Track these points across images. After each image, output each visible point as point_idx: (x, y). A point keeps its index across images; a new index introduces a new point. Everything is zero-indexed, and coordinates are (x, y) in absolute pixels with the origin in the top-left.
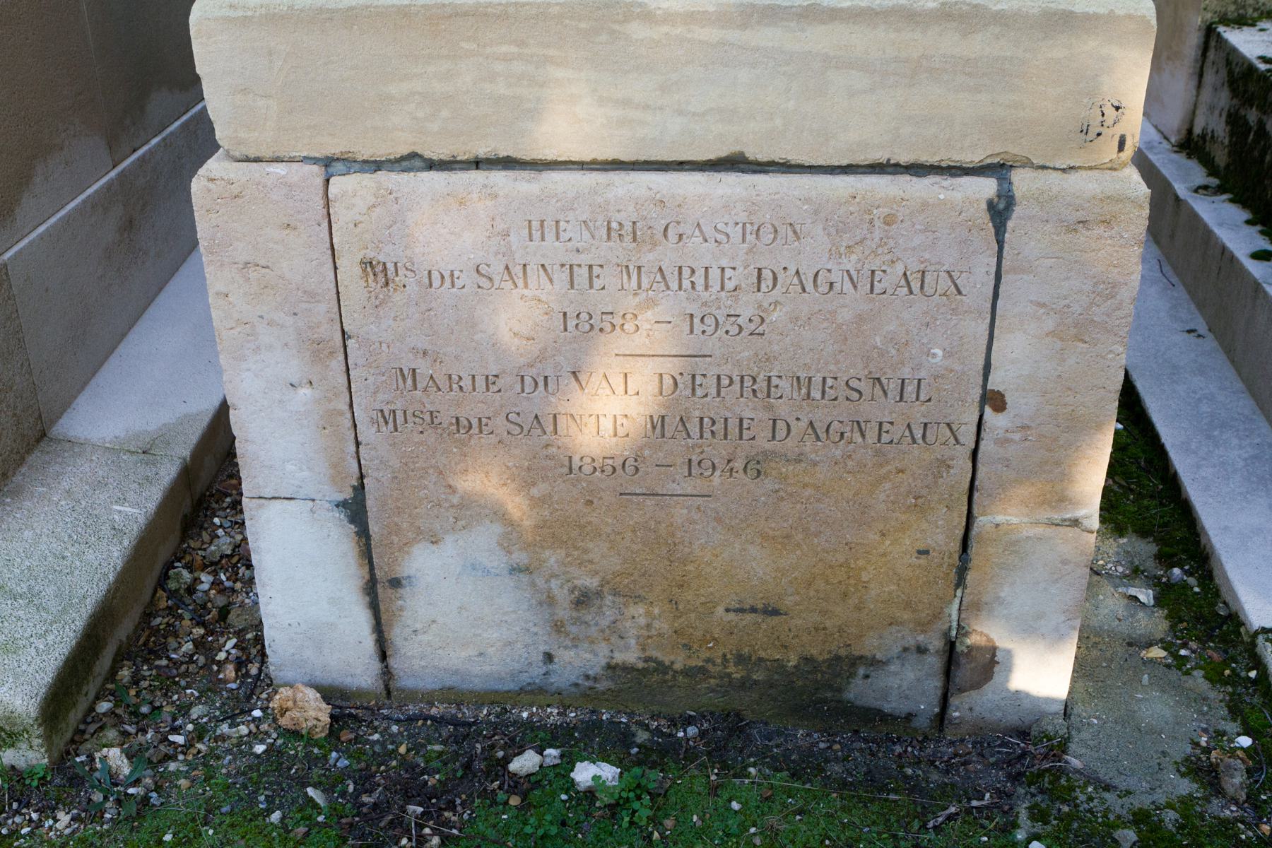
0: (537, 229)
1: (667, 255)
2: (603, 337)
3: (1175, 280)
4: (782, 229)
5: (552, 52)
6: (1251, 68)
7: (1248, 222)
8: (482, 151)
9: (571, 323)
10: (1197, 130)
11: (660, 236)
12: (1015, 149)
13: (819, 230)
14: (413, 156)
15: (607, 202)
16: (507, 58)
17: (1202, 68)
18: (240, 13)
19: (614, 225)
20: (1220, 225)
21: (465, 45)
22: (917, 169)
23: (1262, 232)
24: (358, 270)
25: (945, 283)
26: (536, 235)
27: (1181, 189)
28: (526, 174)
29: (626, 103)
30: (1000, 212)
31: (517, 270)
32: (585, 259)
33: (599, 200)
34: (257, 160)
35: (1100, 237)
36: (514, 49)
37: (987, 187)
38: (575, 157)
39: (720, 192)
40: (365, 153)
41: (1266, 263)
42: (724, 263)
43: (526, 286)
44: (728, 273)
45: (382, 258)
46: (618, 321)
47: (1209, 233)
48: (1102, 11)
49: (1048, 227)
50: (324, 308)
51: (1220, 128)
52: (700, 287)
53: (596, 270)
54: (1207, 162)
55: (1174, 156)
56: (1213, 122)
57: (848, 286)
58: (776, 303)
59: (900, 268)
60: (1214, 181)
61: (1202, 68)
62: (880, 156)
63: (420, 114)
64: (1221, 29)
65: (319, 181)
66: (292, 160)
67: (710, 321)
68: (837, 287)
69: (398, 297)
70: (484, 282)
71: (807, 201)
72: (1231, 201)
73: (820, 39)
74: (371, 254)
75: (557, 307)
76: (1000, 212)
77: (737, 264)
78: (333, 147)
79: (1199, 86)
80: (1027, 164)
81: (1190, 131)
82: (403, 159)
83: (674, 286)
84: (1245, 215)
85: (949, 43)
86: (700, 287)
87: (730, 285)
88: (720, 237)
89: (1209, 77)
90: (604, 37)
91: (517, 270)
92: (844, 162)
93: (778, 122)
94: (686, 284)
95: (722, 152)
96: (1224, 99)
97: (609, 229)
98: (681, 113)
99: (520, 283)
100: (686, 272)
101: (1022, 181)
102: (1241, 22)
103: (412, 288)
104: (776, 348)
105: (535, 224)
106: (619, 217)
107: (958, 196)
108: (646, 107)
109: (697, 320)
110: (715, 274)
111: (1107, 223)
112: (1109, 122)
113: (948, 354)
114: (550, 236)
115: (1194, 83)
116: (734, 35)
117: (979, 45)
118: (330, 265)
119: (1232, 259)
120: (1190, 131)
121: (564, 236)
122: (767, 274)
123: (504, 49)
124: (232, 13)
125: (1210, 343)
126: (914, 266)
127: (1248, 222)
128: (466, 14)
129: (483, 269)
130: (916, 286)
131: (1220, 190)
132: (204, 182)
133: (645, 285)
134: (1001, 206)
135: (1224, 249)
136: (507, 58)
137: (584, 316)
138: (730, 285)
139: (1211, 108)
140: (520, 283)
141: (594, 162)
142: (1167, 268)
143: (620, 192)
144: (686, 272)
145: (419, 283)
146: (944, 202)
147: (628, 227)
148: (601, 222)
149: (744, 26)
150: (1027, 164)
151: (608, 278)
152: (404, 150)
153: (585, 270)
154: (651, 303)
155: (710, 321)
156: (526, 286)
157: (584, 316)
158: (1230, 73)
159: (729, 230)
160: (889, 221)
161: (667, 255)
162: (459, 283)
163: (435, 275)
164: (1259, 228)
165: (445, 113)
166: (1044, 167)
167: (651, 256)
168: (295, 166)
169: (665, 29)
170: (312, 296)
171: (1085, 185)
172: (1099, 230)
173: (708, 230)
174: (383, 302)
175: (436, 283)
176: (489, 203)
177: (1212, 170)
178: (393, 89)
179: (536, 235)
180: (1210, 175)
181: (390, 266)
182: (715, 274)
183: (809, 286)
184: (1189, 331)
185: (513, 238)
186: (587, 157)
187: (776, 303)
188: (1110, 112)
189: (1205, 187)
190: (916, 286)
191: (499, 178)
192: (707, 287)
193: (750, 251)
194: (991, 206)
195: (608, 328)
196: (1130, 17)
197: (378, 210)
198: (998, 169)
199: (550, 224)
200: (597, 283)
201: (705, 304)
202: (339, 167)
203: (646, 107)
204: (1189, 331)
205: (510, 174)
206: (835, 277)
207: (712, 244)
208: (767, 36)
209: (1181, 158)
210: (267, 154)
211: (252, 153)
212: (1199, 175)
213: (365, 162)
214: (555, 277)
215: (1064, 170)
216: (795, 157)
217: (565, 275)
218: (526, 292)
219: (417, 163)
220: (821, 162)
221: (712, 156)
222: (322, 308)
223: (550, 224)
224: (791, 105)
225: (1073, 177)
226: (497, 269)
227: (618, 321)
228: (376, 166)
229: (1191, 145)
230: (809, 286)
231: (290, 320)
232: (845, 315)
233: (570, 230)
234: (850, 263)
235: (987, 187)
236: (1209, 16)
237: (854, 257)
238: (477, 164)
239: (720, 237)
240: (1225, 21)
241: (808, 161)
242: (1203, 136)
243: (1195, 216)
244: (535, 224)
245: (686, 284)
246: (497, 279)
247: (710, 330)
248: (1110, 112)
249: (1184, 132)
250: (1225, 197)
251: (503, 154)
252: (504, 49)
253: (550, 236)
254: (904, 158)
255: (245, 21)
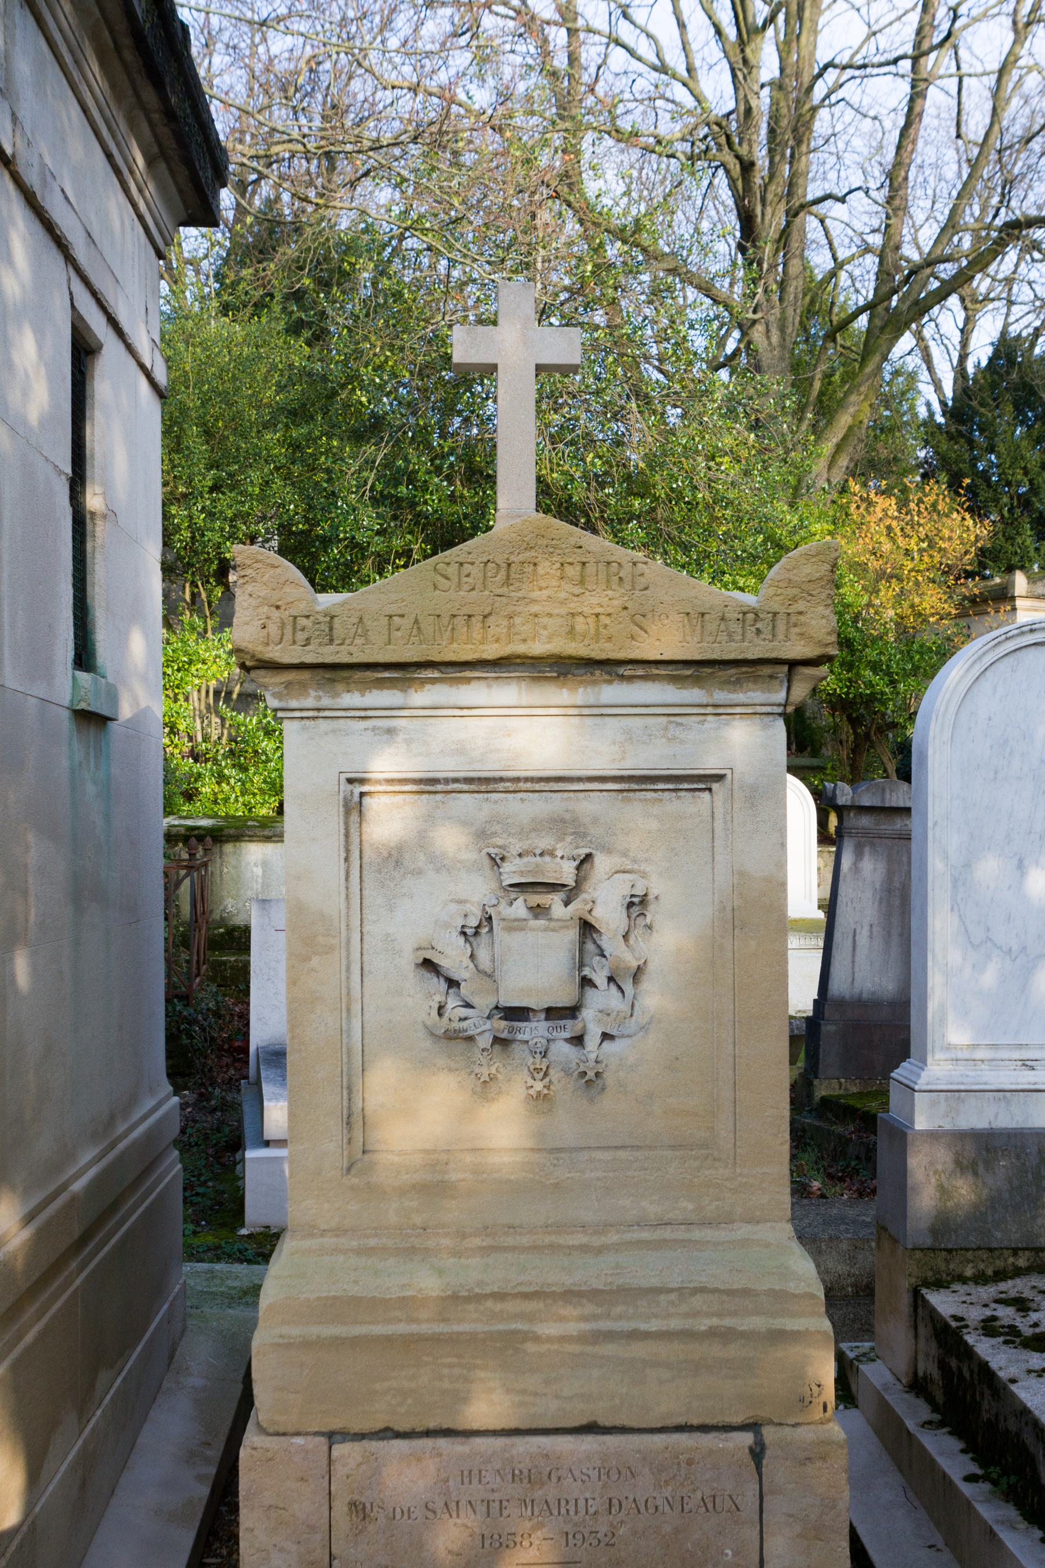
0: (467, 1476)
1: (550, 1492)
2: (508, 1551)
3: (916, 1503)
4: (623, 1471)
5: (479, 1362)
6: (947, 1325)
7: (963, 1451)
8: (432, 1424)
9: (487, 1542)
10: (921, 1374)
11: (545, 1478)
12: (763, 1413)
13: (647, 1470)
14: (387, 1429)
15: (512, 1457)
16: (451, 1366)
17: (915, 1321)
18: (286, 1341)
19: (517, 1472)
20: (941, 1454)
21: (425, 1358)
22: (704, 1428)
23: (973, 1459)
24: (346, 1509)
25: (728, 1503)
26: (466, 1480)
27: (910, 1424)
28: (459, 1440)
29: (524, 1392)
30: (757, 1453)
31: (453, 1506)
32: (497, 1496)
33: (507, 1455)
34: (284, 1434)
35: (820, 1469)
36: (455, 1360)
37: (747, 1439)
38: (491, 1427)
39: (583, 1448)
40: (356, 1427)
41: (975, 1484)
42: (588, 1495)
43: (458, 1516)
44: (590, 1502)
45: (363, 1500)
46: (518, 1539)
47: (933, 1461)
48: (802, 1329)
49: (788, 1463)
50: (318, 1539)
51: (935, 1373)
52: (572, 1513)
53: (505, 1503)
54: (930, 1400)
55: (906, 1396)
56: (928, 1367)
57: (667, 1508)
58: (622, 1522)
59: (699, 1495)
60: (937, 1417)
61: (915, 1321)
62: (681, 1420)
63: (394, 1402)
64: (924, 1291)
65: (325, 1448)
66: (307, 1434)
67: (579, 1536)
68: (660, 1508)
69: (371, 1528)
70: (430, 1515)
71: (639, 1451)
72: (950, 1433)
73: (640, 1350)
74: (356, 1497)
75: (477, 1531)
76: (757, 1453)
77: (596, 1495)
78: (336, 1424)
79: (916, 1336)
80: (770, 1422)
81: (915, 1373)
82: (380, 1431)
83: (556, 1512)
84: (960, 1445)
85: (715, 1350)
86: (572, 1513)
87: (591, 1510)
88: (584, 1478)
89: (922, 1330)
90: (510, 1352)
91: (453, 1506)
92: (659, 1425)
93: (617, 1401)
94: (563, 1511)
95: (584, 1421)
96: (933, 1349)
97: (513, 1475)
98: (557, 1397)
99: (454, 1515)
100: (563, 1503)
101: (769, 1434)
102: (939, 1284)
103: (382, 1520)
104: (623, 1554)
105: (466, 1473)
106: (520, 1466)
107: (730, 1445)
108: (536, 1394)
109: (570, 1537)
110: (582, 1503)
111: (824, 1459)
112: (815, 1394)
113: (736, 1554)
114: (475, 1481)
115: (911, 1334)
116: (589, 1349)
117: (734, 1351)
118: (327, 1506)
119: (951, 1482)
120: (915, 1373)
121: (485, 1481)
122: (615, 1502)
123: (449, 1360)
124: (281, 1341)
125: (947, 1556)
126: (708, 1492)
127: (963, 1451)
128: (427, 1340)
129: (430, 1507)
130: (710, 1506)
131: (941, 1424)
132: (249, 1450)
133: (536, 1513)
134: (758, 1450)
135: (945, 1475)
136: (451, 1366)
137: (496, 1537)
138: (591, 1510)
139: (927, 1355)
140: (454, 1515)
141: (503, 1430)
142: (910, 1494)
143: (521, 1449)
144: (563, 1503)
145: (387, 1517)
146: (723, 1449)
147: (525, 1472)
148: (508, 1470)
149: (594, 1343)
150: (770, 1422)
151: (512, 1510)
152: (380, 1426)
153: (497, 1504)
154: (540, 1526)
155: (579, 1536)
156: (458, 1516)
157: (496, 1537)
158: (935, 1328)
159: (590, 1473)
160: (690, 1462)
161: (550, 1492)
162: (413, 1516)
163: (398, 1510)
164: (970, 1455)
165: (410, 1401)
166: (781, 1424)
167: (540, 1493)
168: (309, 1438)
169: (547, 1346)
170: (312, 1529)
171: (805, 1434)
172: (819, 1464)
173: (576, 1473)
174: (361, 1531)
175: (398, 1516)
176: (437, 1460)
177: (935, 1409)
178: (378, 1386)
179: (466, 1480)
180: (933, 1411)
181: (368, 1505)
182: (582, 1503)
183: (642, 1509)
184: (930, 1547)
185: (451, 1483)
186: (499, 1427)
187: (622, 1522)
188: (815, 1388)
189: (930, 1423)
190: (710, 1506)
191: (442, 1443)
192: (576, 1513)
193: (604, 1486)
194: (751, 1450)
195: (512, 1545)
196: (818, 1332)
197: (364, 1467)
198: (753, 1426)
199: (475, 1472)
200: (505, 1513)
201: (576, 1524)
202: (338, 1437)
203: (536, 1394)
204: (930, 1547)
205: (449, 1439)
206: (659, 1502)
207: (579, 1483)
208: (608, 1349)
209: (910, 1397)
210: (292, 1430)
211: (282, 1430)
212: (925, 1412)
213: (355, 1434)
214: (478, 1509)
215: (793, 1426)
216: (628, 1423)
217: (484, 1509)
218: (458, 1521)
219: (389, 1434)
220: (644, 1426)
221: (577, 1424)
222: (318, 1537)
223: (475, 1472)
224: (624, 1390)
225: (799, 1430)
226: (439, 1504)
227: (518, 1539)
228: (361, 1436)
229: (917, 1386)
230: (642, 1509)
231: (294, 1548)
232: (667, 1529)
233: (488, 1477)
234: (667, 1492)
235: (747, 1439)
236: (913, 1280)
237: (670, 1488)
238: (428, 1433)
239: (584, 1478)
240: (927, 1284)
241: (635, 1424)
242: (925, 1378)
243: (923, 1448)
244: (466, 1473)
245: (563, 1511)
246: (439, 1512)
247: (579, 1543)
248: (815, 1388)
249: (911, 1375)
250: (945, 1430)
251: (445, 1426)
252: (449, 1360)
253: (475, 1481)
254: (695, 1422)
255: (289, 1346)
